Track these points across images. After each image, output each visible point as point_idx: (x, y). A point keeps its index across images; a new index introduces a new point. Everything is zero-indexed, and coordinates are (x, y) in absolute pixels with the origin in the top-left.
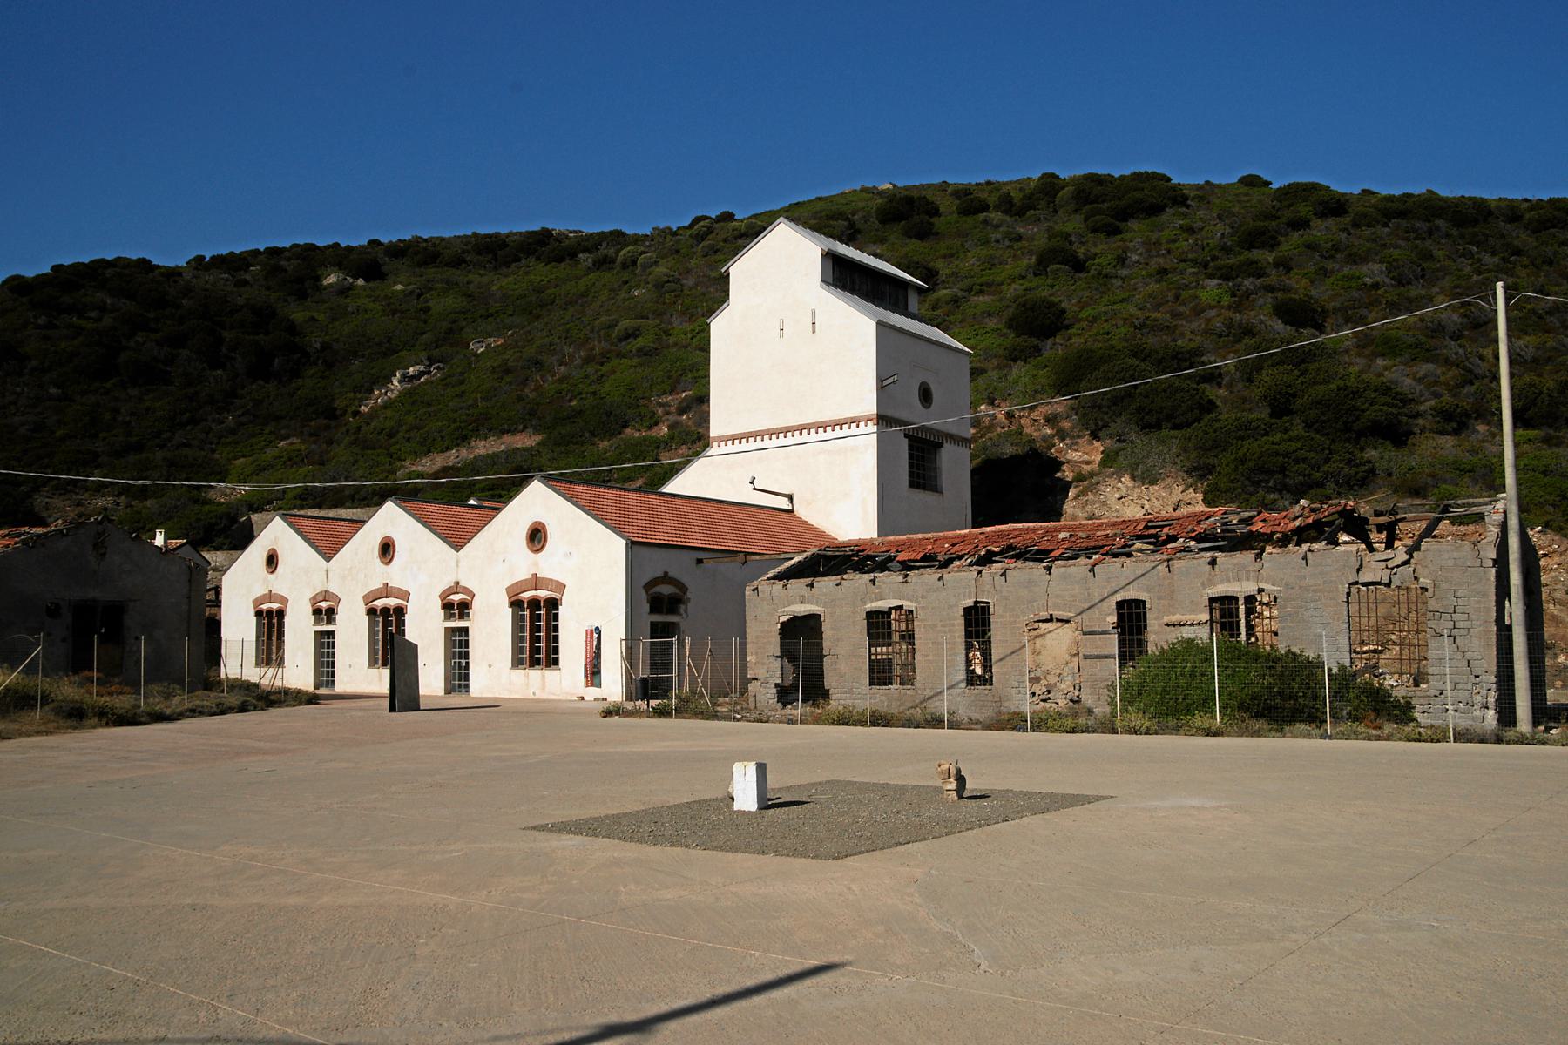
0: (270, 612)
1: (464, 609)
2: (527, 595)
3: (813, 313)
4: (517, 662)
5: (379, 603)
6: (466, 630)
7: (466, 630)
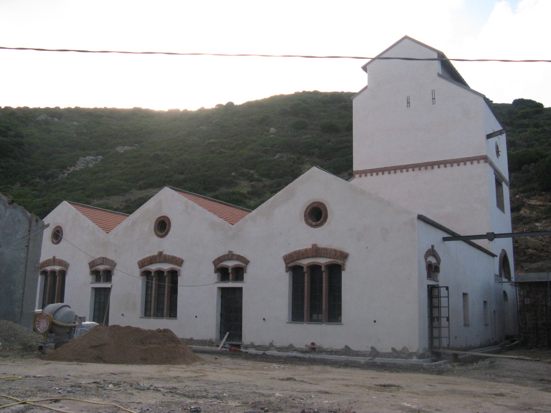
0: (160, 273)
1: (239, 273)
2: (305, 262)
3: (433, 92)
4: (297, 315)
5: (153, 267)
6: (240, 289)
7: (240, 289)
